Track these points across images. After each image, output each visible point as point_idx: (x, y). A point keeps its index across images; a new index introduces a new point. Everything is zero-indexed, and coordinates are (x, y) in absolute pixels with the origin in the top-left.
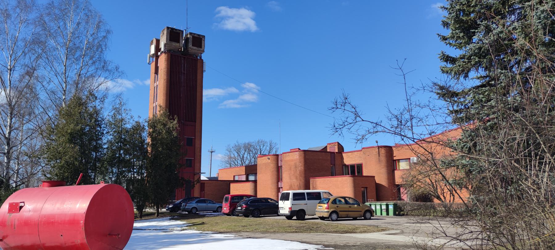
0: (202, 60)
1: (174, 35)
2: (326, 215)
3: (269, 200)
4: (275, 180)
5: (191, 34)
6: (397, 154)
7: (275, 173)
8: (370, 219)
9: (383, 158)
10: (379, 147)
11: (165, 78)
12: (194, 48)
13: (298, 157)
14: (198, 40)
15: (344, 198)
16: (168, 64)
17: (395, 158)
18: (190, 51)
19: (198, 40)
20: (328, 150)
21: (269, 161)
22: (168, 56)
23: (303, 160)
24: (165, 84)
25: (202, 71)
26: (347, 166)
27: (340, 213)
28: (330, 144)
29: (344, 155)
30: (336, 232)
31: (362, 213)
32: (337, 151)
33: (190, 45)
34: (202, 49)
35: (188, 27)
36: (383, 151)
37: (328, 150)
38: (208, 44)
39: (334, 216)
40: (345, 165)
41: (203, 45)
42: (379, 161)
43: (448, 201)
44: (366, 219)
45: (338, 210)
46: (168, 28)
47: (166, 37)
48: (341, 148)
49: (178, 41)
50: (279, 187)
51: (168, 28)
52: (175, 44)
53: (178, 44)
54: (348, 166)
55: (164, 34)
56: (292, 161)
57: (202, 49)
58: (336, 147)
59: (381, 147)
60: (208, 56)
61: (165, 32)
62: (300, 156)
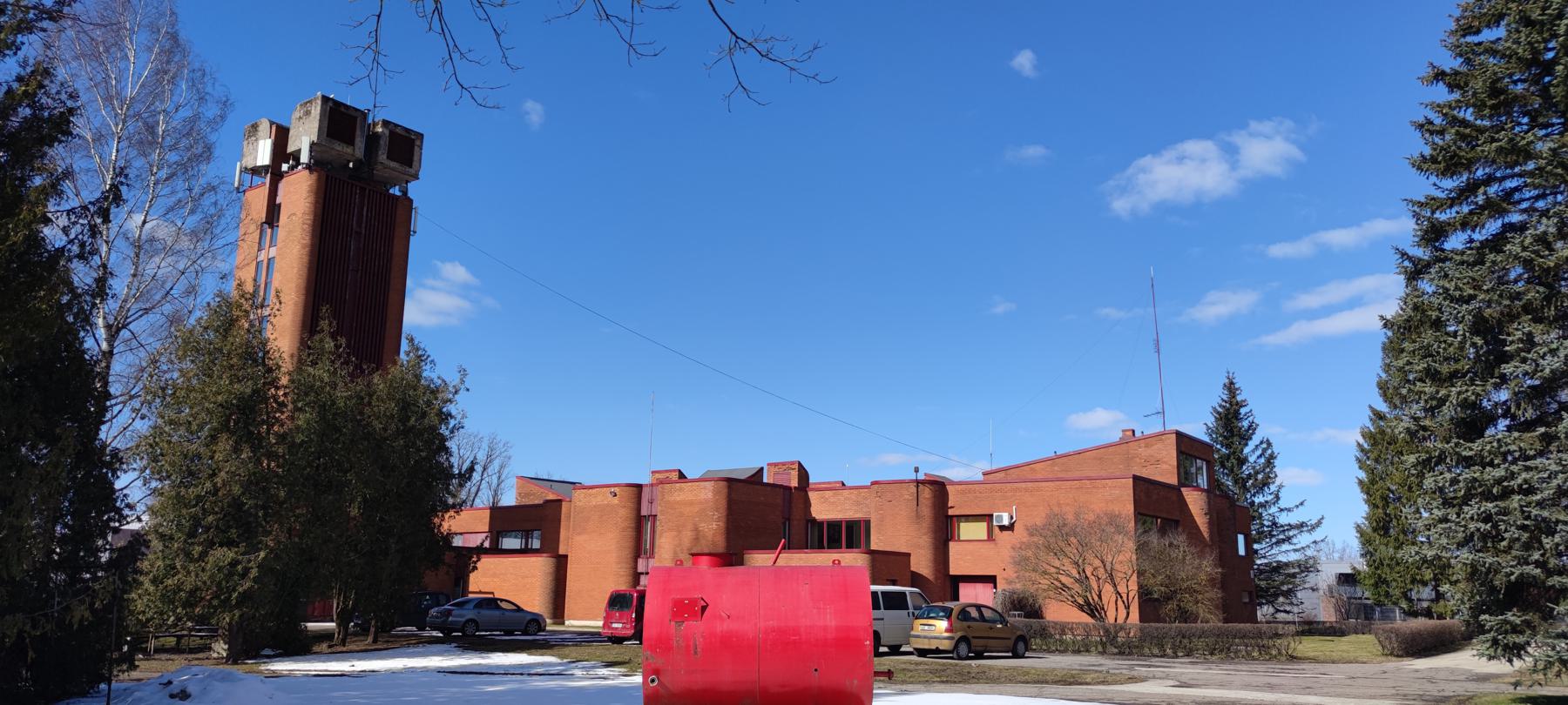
0: (411, 201)
1: (340, 121)
2: (946, 645)
3: (503, 605)
4: (627, 554)
5: (386, 123)
6: (956, 505)
7: (630, 533)
8: (1023, 657)
9: (926, 511)
10: (918, 482)
11: (307, 240)
12: (393, 164)
13: (710, 495)
14: (405, 145)
15: (979, 607)
16: (317, 202)
17: (951, 512)
18: (379, 172)
19: (405, 145)
20: (765, 480)
21: (616, 501)
22: (319, 180)
23: (723, 503)
24: (306, 259)
25: (407, 234)
26: (819, 524)
27: (974, 642)
28: (776, 465)
29: (811, 494)
30: (1056, 682)
31: (1011, 643)
32: (794, 483)
33: (382, 157)
34: (412, 171)
35: (387, 106)
36: (926, 493)
37: (765, 480)
38: (429, 156)
39: (963, 649)
40: (814, 520)
41: (416, 158)
42: (918, 516)
43: (1112, 621)
44: (1016, 656)
45: (970, 635)
46: (325, 99)
47: (317, 125)
48: (803, 474)
49: (350, 142)
50: (640, 569)
51: (325, 99)
52: (340, 148)
53: (349, 150)
54: (821, 524)
55: (308, 113)
56: (691, 503)
57: (412, 171)
58: (795, 474)
59: (923, 482)
60: (425, 191)
61: (316, 110)
62: (716, 492)
